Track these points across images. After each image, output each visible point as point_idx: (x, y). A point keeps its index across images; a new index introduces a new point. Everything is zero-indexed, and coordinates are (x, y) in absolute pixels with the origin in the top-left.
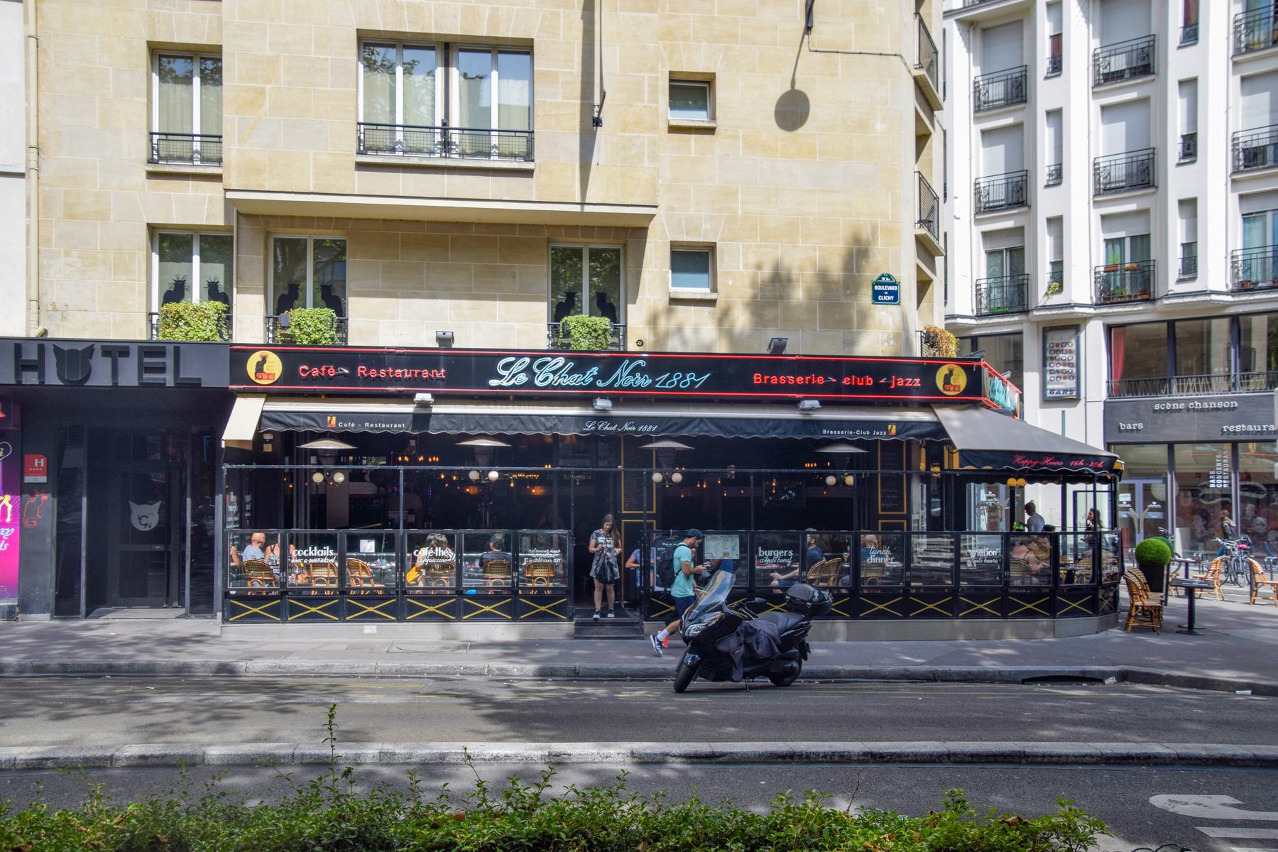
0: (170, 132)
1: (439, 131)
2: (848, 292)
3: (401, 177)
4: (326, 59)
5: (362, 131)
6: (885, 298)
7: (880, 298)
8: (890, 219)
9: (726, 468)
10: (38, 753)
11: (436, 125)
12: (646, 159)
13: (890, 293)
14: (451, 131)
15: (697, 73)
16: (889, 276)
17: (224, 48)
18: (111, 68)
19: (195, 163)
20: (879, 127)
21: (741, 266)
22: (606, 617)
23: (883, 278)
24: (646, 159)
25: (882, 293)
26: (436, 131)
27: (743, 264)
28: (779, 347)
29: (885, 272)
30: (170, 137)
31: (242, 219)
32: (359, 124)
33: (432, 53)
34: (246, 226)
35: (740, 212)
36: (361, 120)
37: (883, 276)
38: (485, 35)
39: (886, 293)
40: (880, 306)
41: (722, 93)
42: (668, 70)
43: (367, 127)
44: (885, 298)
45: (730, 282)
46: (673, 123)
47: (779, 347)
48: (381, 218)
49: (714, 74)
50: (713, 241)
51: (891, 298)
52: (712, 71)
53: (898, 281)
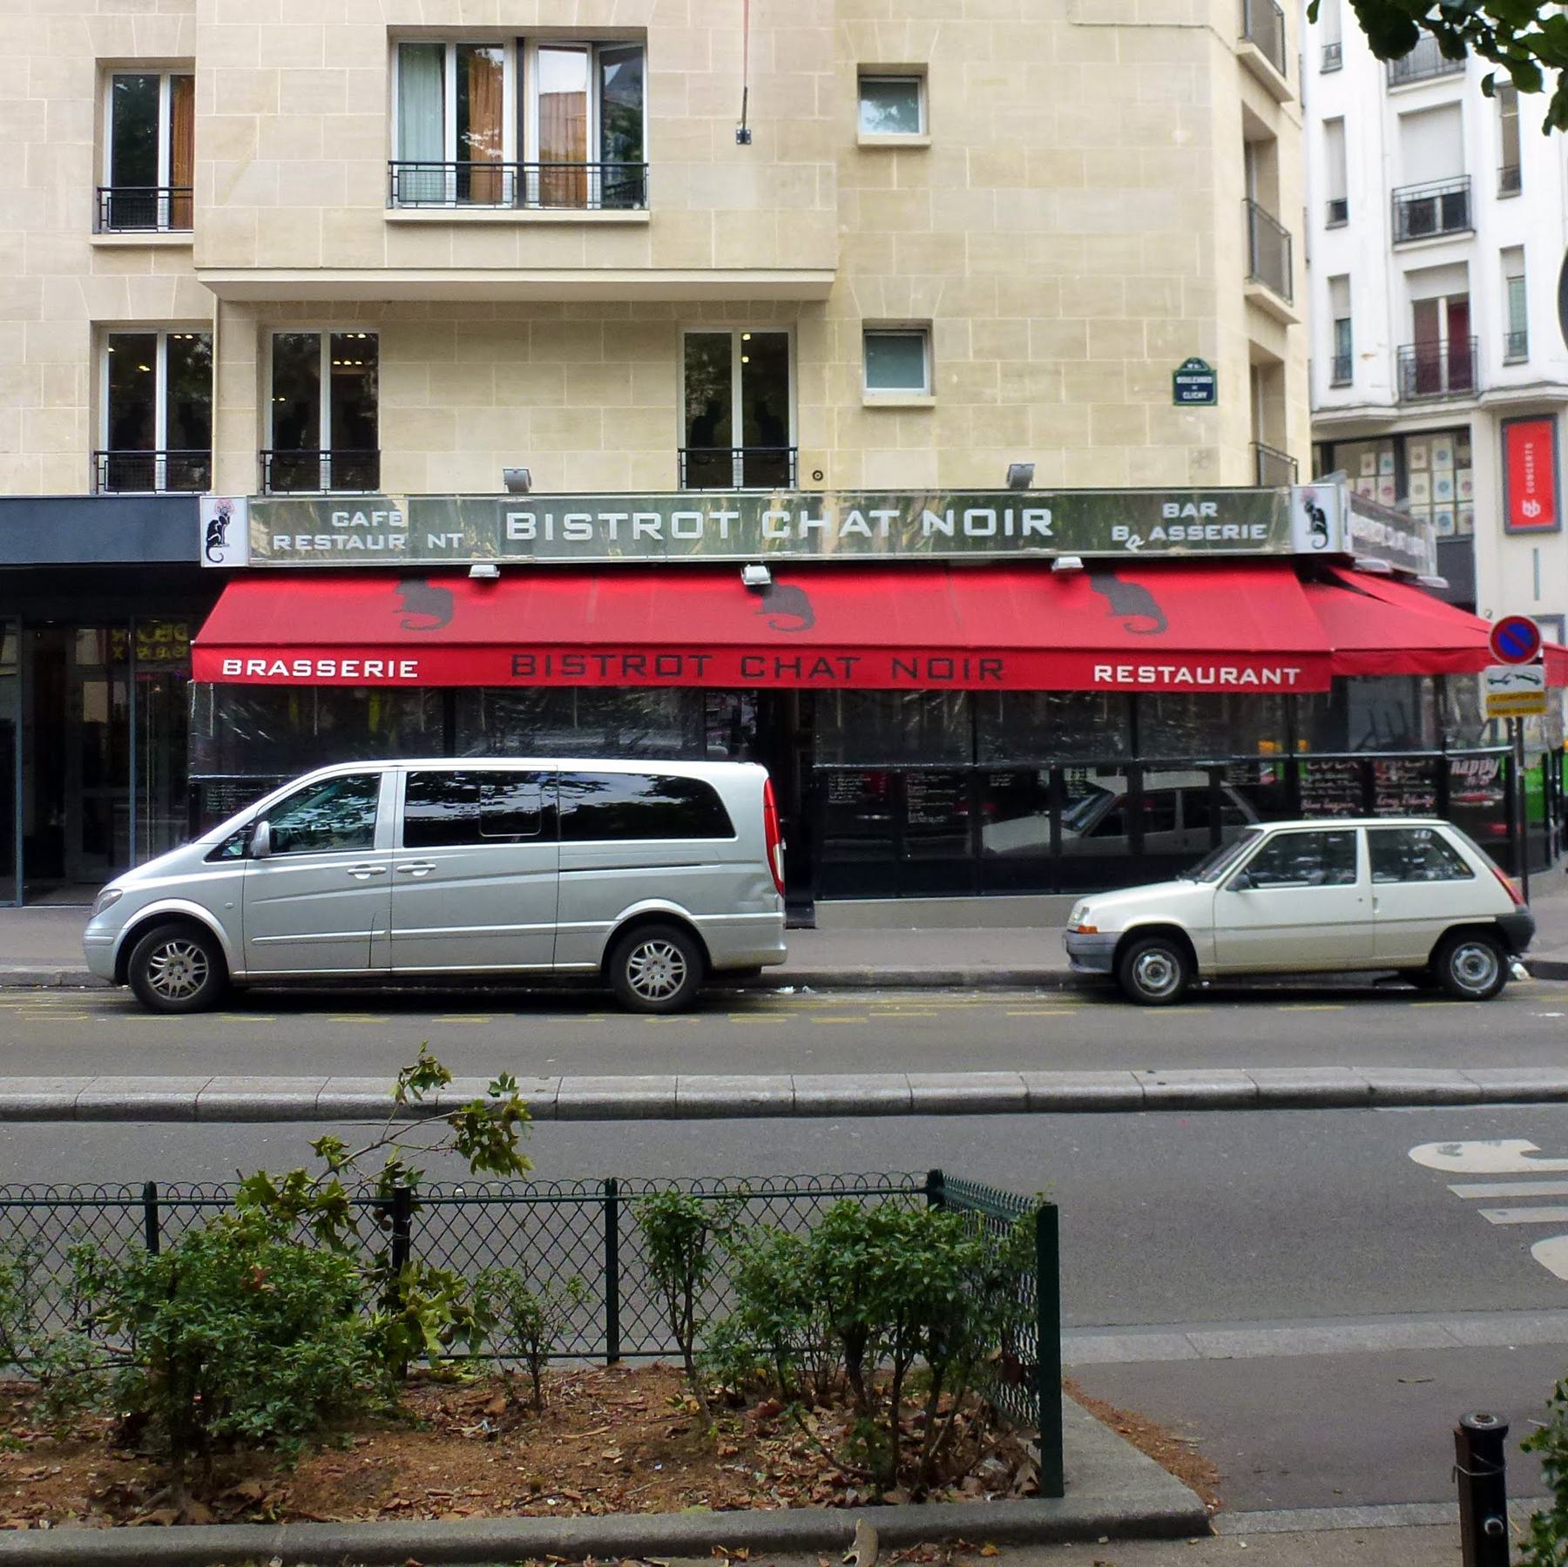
0: (422, 160)
1: (453, 168)
2: (1136, 389)
3: (452, 239)
4: (343, 72)
5: (395, 174)
6: (1195, 395)
7: (1186, 395)
8: (1198, 274)
9: (1546, 65)
10: (90, 1002)
11: (447, 160)
12: (817, 199)
13: (1202, 387)
14: (526, 169)
15: (900, 65)
16: (1199, 362)
17: (930, 67)
18: (46, 101)
19: (160, 229)
20: (1180, 135)
21: (971, 354)
22: (1084, 560)
23: (1190, 366)
24: (817, 199)
25: (1188, 387)
26: (448, 168)
27: (975, 352)
28: (1020, 480)
29: (1190, 355)
30: (421, 167)
31: (226, 308)
32: (391, 163)
33: (584, 56)
34: (231, 319)
35: (968, 274)
36: (395, 159)
37: (1189, 361)
38: (574, 25)
39: (1195, 388)
40: (1185, 408)
41: (937, 91)
42: (856, 61)
43: (402, 167)
44: (1195, 395)
45: (955, 379)
46: (863, 141)
47: (1020, 480)
48: (428, 299)
49: (925, 66)
50: (926, 316)
51: (1203, 395)
52: (922, 61)
53: (1213, 368)
